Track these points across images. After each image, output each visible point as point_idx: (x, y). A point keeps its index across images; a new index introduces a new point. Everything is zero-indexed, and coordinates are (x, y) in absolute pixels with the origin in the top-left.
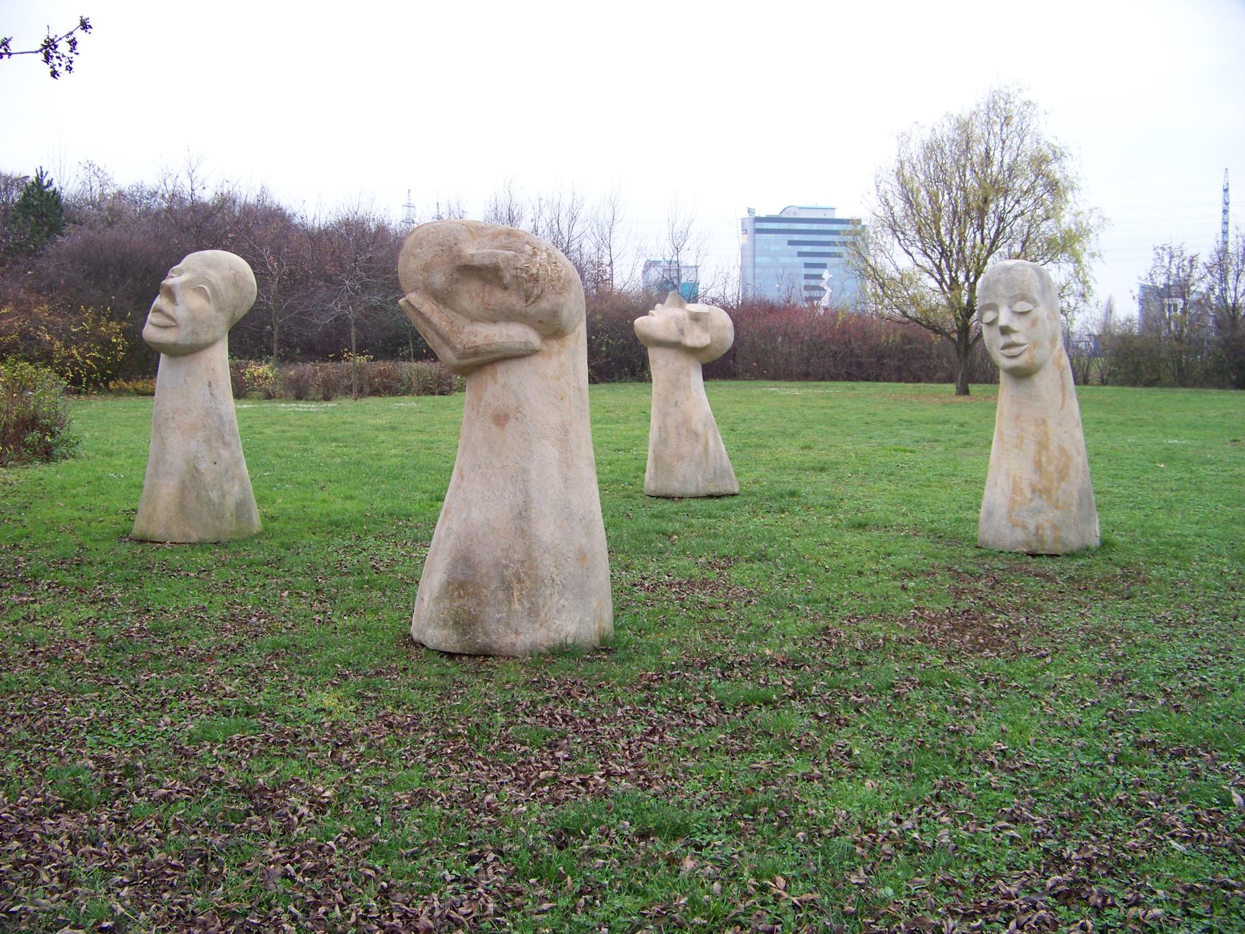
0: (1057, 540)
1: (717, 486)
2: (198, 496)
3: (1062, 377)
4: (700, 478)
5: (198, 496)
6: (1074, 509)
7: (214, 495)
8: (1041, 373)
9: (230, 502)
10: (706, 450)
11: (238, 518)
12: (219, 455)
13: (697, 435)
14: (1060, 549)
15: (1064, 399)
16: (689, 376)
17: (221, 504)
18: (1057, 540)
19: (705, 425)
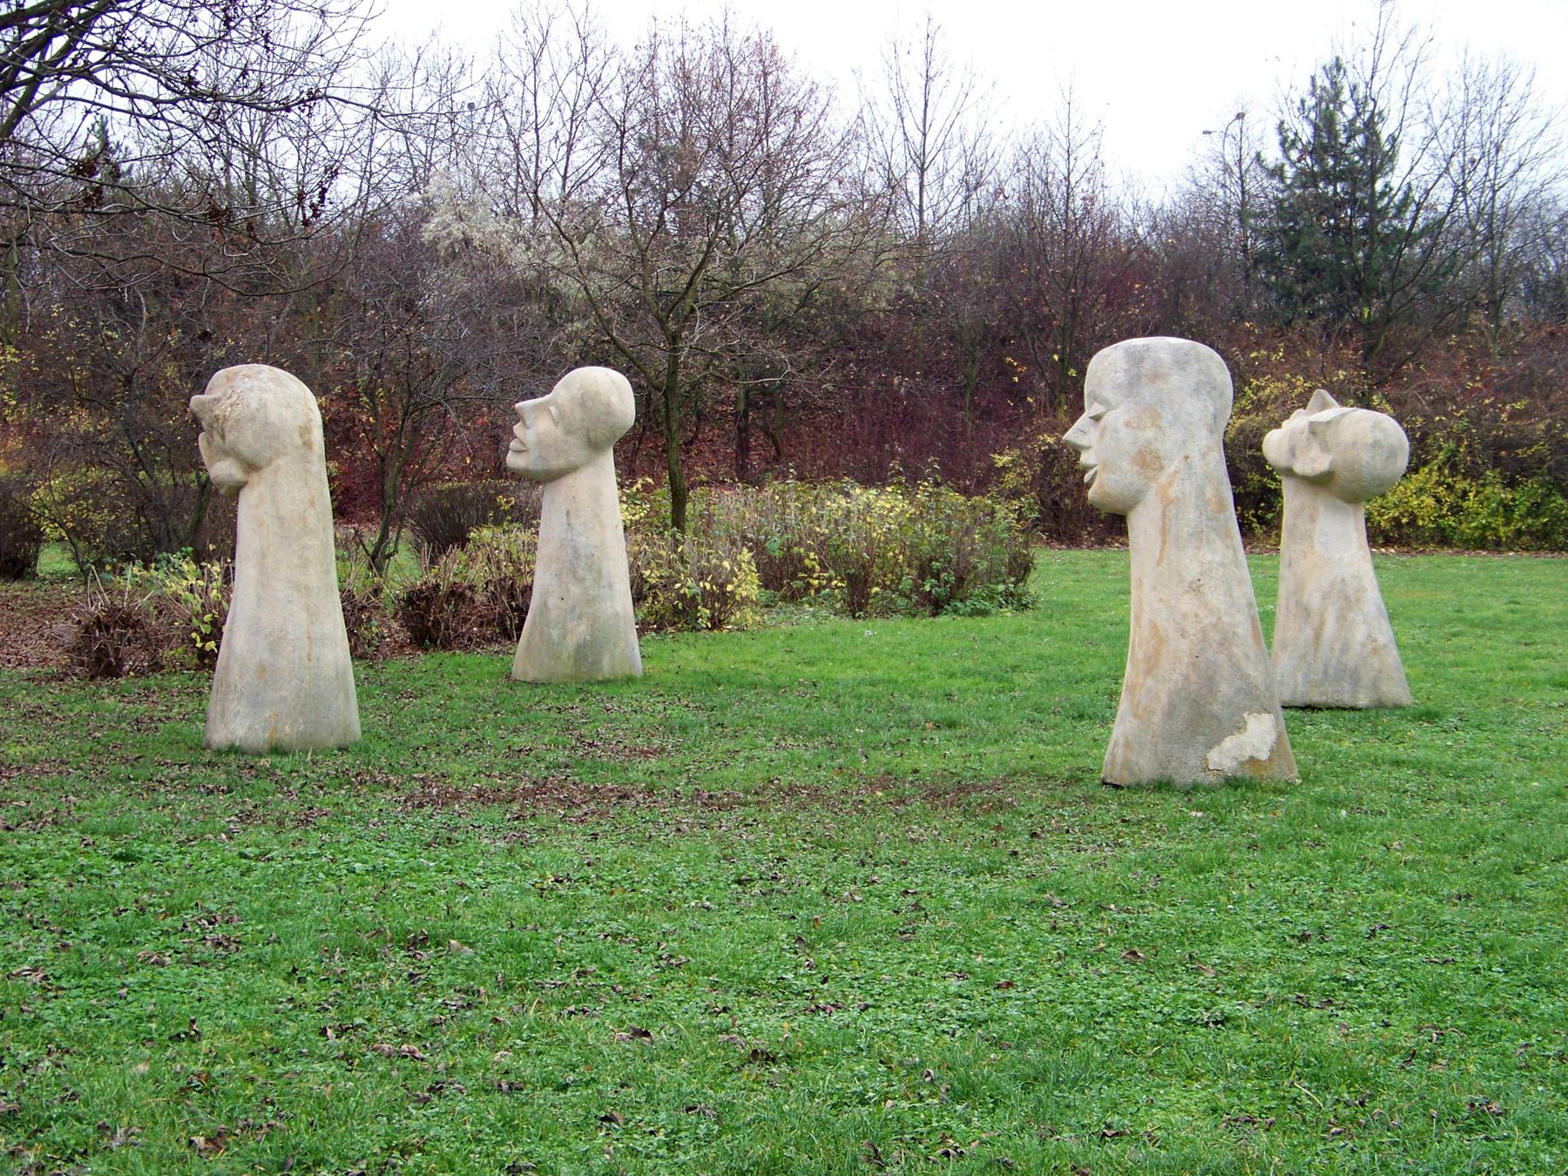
0: (1126, 764)
1: (1323, 694)
2: (542, 633)
3: (1164, 515)
4: (1300, 678)
5: (542, 633)
6: (1156, 719)
7: (555, 634)
8: (1139, 508)
9: (571, 643)
10: (1318, 637)
11: (576, 660)
12: (568, 591)
13: (1307, 611)
14: (1124, 778)
15: (1162, 550)
16: (1312, 519)
17: (560, 644)
18: (1126, 764)
19: (1325, 597)
